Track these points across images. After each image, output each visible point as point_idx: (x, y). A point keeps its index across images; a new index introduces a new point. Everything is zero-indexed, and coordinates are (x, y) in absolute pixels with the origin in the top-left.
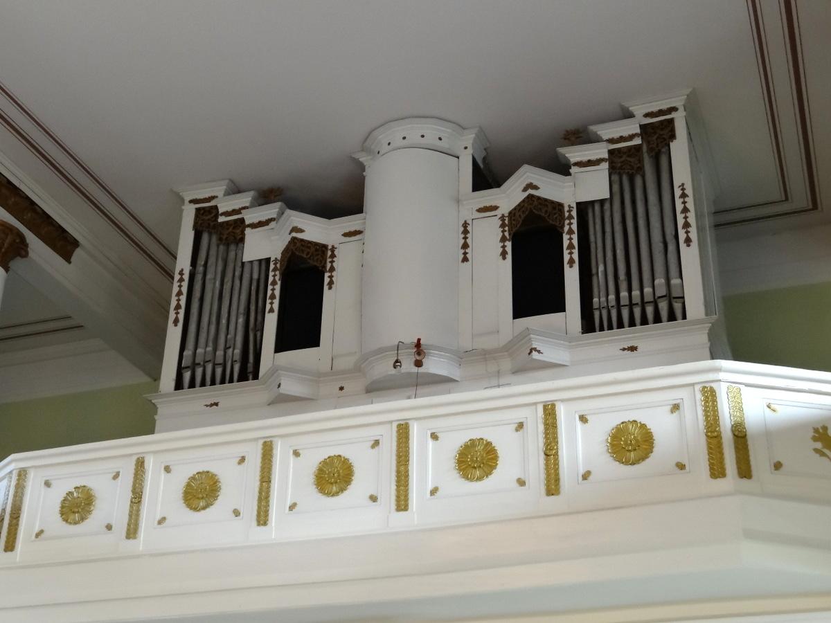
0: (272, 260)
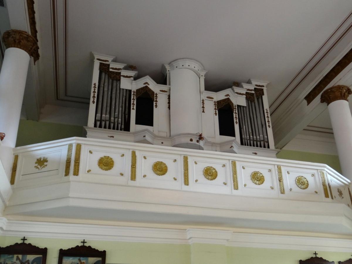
0: (132, 91)
